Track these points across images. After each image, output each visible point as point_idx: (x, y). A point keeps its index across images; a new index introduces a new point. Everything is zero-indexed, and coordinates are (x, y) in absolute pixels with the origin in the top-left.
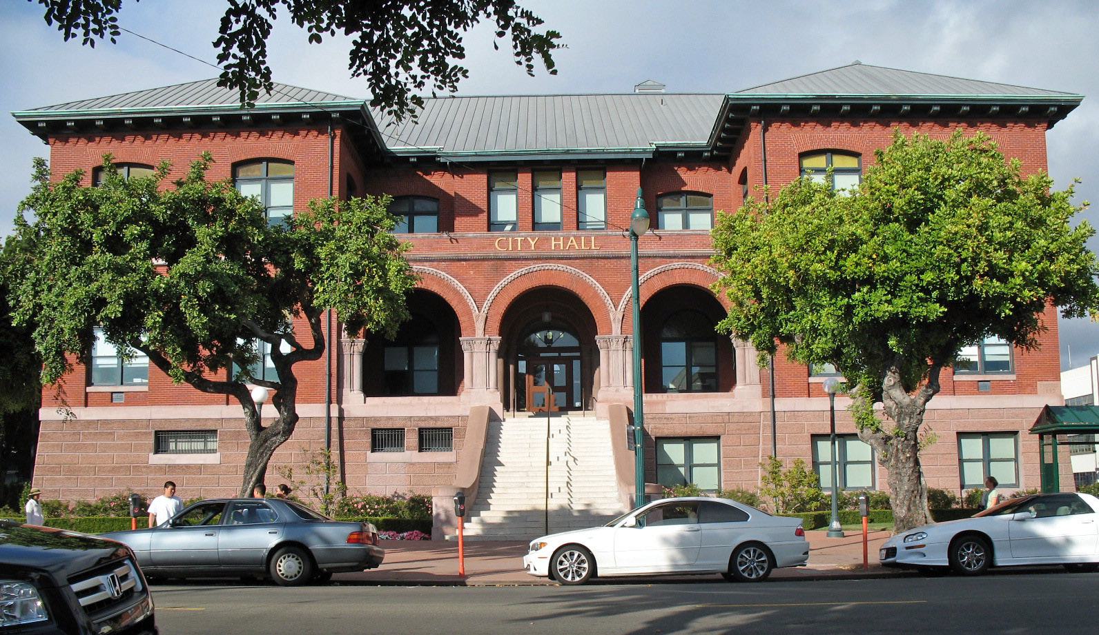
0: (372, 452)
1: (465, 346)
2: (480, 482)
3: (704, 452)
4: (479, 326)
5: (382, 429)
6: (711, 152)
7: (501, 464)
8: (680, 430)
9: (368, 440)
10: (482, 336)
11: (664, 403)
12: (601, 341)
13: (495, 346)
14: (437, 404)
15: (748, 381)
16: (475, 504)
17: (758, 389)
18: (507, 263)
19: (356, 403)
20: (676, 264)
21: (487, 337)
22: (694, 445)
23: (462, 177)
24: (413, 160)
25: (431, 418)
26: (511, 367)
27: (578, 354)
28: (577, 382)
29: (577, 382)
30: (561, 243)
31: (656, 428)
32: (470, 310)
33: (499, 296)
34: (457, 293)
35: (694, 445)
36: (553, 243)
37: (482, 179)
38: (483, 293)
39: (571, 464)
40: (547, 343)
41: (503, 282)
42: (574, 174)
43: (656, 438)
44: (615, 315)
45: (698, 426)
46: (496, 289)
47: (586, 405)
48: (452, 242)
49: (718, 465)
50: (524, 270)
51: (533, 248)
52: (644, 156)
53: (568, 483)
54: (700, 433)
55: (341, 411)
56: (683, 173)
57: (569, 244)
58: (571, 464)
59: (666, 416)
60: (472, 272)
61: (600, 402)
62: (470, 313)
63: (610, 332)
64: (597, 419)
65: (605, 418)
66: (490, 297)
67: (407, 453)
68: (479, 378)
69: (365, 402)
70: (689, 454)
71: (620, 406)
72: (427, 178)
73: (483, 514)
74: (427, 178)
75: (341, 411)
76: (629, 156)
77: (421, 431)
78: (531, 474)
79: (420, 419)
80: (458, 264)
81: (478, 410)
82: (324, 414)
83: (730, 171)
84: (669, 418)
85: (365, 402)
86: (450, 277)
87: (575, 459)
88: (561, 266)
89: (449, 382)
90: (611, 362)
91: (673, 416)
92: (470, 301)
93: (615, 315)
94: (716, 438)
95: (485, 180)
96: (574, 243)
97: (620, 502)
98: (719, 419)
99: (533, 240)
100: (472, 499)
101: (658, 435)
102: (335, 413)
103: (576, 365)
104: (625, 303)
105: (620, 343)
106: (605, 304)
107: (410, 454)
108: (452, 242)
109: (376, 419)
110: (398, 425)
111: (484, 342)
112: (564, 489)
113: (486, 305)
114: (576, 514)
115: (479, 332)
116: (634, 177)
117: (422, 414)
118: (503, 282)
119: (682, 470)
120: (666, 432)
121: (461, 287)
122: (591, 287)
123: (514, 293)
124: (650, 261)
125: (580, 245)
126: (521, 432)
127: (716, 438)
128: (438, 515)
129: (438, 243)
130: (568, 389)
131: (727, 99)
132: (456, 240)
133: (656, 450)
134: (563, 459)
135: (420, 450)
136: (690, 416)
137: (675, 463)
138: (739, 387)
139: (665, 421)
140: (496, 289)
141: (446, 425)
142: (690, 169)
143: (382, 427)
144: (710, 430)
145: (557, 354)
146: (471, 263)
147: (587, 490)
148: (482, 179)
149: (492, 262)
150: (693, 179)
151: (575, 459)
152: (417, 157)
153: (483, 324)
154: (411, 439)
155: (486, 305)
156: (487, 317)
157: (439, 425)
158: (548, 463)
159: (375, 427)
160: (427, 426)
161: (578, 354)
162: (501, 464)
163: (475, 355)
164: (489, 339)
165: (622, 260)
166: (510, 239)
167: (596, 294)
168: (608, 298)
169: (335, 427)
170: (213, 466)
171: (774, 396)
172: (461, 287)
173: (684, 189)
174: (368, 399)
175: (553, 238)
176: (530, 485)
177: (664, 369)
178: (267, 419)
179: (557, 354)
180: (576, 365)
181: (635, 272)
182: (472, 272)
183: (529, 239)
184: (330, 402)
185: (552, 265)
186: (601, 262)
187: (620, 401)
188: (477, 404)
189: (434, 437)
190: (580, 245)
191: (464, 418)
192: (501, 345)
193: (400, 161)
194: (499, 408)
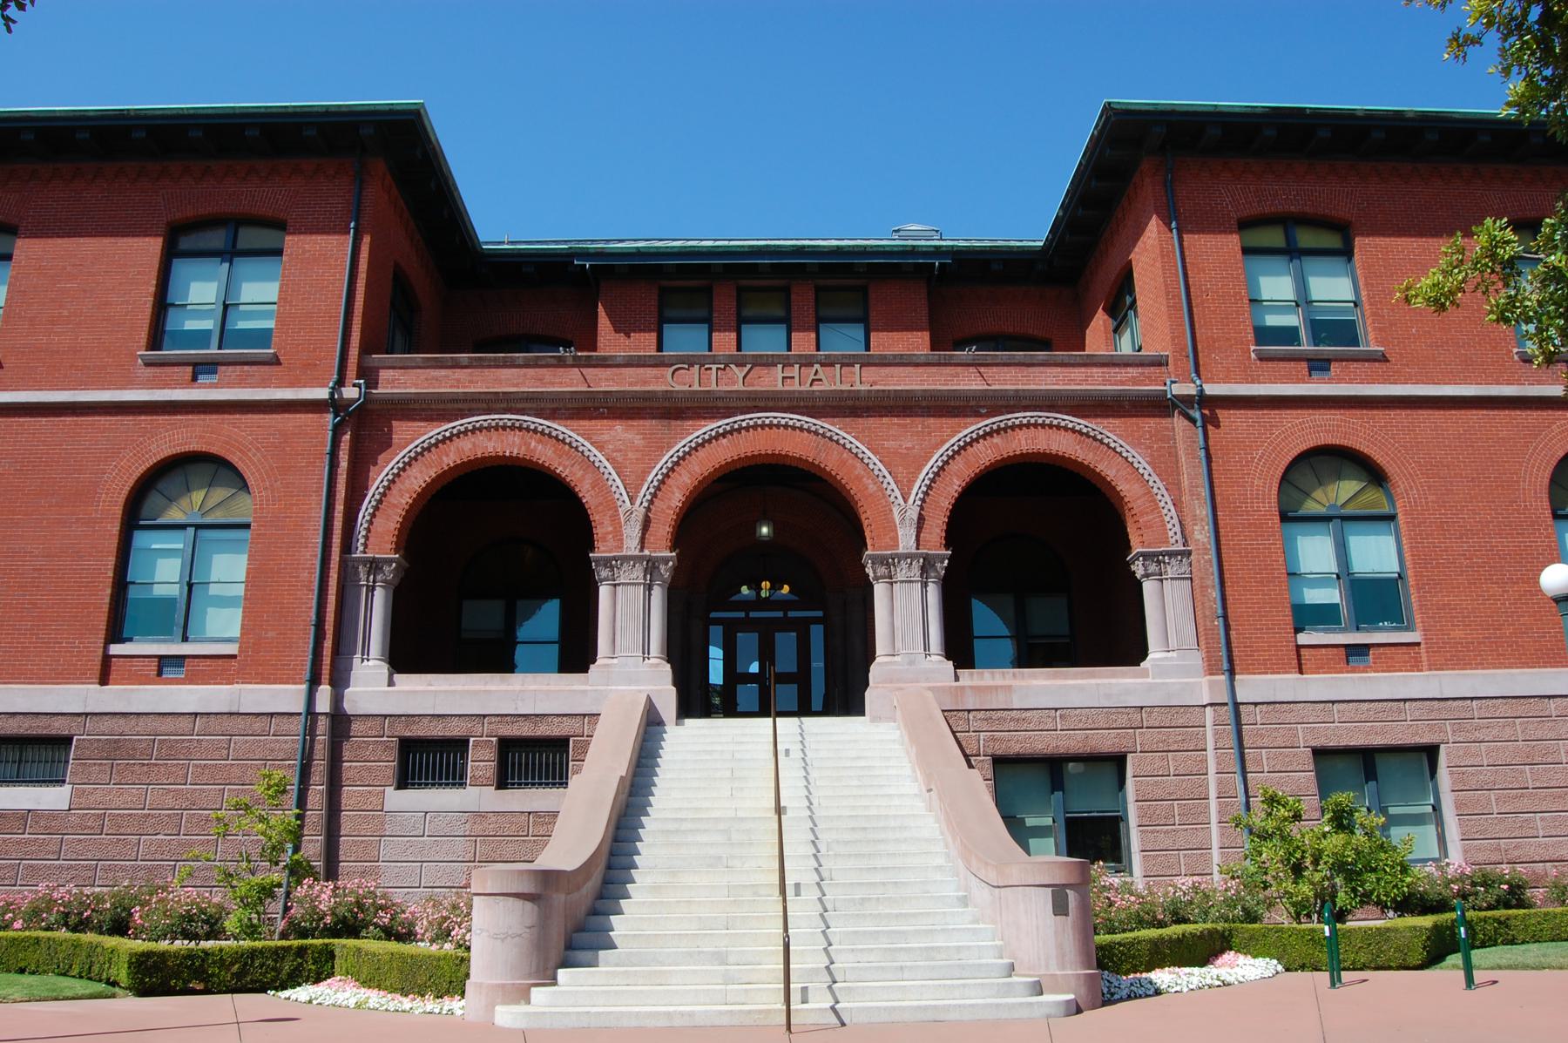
0: (399, 788)
4: (632, 533)
9: (388, 765)
15: (1173, 643)
17: (1196, 659)
19: (373, 687)
27: (820, 614)
31: (994, 739)
32: (614, 501)
46: (666, 460)
55: (337, 700)
66: (653, 476)
68: (630, 636)
75: (337, 700)
82: (300, 707)
89: (577, 653)
98: (1122, 720)
102: (323, 704)
103: (817, 632)
107: (476, 796)
110: (455, 730)
122: (859, 456)
126: (719, 760)
135: (502, 784)
138: (1155, 654)
145: (780, 614)
154: (481, 761)
155: (645, 491)
157: (543, 730)
161: (820, 614)
169: (322, 738)
170: (53, 815)
171: (1232, 672)
174: (397, 677)
178: (1455, 967)
179: (780, 614)
180: (817, 632)
181: (778, 898)
184: (314, 681)
189: (536, 758)
194: (667, 700)
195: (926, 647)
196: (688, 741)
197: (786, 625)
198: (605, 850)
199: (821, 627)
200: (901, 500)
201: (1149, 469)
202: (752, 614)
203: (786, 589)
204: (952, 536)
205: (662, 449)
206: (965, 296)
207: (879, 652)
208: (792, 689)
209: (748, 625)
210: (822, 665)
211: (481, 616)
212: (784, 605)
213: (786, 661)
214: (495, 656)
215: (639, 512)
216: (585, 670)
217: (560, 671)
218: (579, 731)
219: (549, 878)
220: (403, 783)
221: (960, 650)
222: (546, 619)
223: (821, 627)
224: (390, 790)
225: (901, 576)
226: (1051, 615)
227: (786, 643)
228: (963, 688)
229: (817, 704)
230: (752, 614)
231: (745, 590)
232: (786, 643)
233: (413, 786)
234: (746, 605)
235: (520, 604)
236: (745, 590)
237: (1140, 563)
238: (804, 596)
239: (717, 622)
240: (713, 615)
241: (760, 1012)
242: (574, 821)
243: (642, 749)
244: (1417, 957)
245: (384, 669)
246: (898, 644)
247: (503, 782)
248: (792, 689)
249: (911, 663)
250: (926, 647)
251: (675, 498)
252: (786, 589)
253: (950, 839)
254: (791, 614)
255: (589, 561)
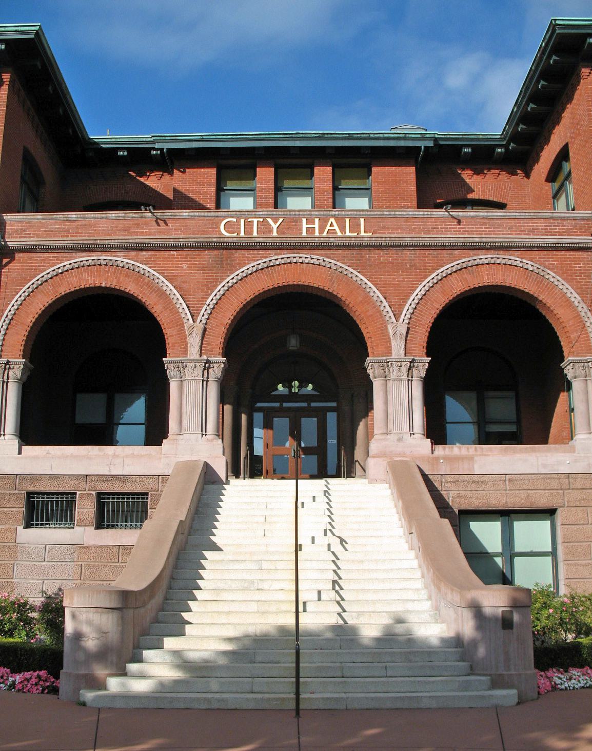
1: (171, 372)
2: (172, 578)
3: (532, 534)
4: (194, 342)
5: (43, 494)
6: (506, 146)
7: (215, 548)
8: (496, 501)
9: (19, 509)
10: (197, 357)
11: (471, 459)
12: (376, 365)
13: (216, 372)
14: (127, 456)
16: (156, 621)
18: (237, 254)
20: (484, 257)
21: (205, 357)
22: (515, 523)
23: (184, 172)
24: (121, 153)
25: (117, 477)
26: (244, 417)
27: (334, 404)
28: (332, 441)
29: (332, 441)
30: (316, 226)
31: (459, 496)
32: (181, 319)
33: (224, 300)
34: (162, 294)
35: (515, 523)
36: (305, 226)
37: (209, 175)
38: (200, 294)
39: (337, 547)
40: (296, 374)
41: (230, 279)
42: (329, 169)
43: (461, 512)
44: (396, 329)
45: (523, 494)
46: (220, 289)
47: (345, 467)
48: (158, 225)
49: (554, 554)
50: (261, 262)
51: (275, 234)
52: (422, 144)
53: (334, 582)
54: (526, 506)
56: (468, 176)
57: (328, 227)
58: (337, 547)
59: (475, 478)
60: (185, 266)
61: (374, 457)
62: (180, 324)
63: (389, 353)
64: (370, 482)
65: (383, 481)
66: (211, 300)
67: (78, 530)
68: (192, 420)
69: (20, 453)
70: (508, 537)
71: (405, 462)
72: (142, 179)
73: (170, 643)
74: (142, 179)
76: (402, 143)
77: (101, 497)
78: (265, 566)
79: (100, 477)
80: (166, 254)
81: (188, 466)
83: (528, 176)
84: (480, 480)
85: (20, 453)
86: (152, 272)
87: (342, 541)
88: (316, 257)
89: (156, 432)
90: (389, 397)
91: (485, 478)
92: (182, 305)
93: (396, 329)
94: (549, 513)
95: (214, 176)
96: (336, 227)
97: (436, 622)
98: (554, 484)
99: (275, 222)
100: (155, 609)
101: (463, 507)
103: (332, 418)
104: (411, 311)
105: (404, 369)
106: (380, 312)
107: (83, 533)
108: (158, 225)
109: (35, 478)
111: (199, 366)
112: (329, 595)
113: (204, 312)
114: (366, 642)
115: (193, 352)
116: (408, 174)
117: (104, 471)
118: (230, 279)
119: (499, 560)
120: (476, 503)
121: (168, 287)
122: (360, 288)
123: (247, 294)
124: (445, 253)
125: (343, 230)
126: (251, 506)
127: (549, 513)
128: (78, 636)
129: (137, 225)
130: (320, 451)
131: (553, 26)
132: (164, 221)
133: (460, 528)
134: (322, 540)
135: (99, 526)
136: (511, 479)
137: (490, 551)
139: (474, 486)
140: (220, 289)
141: (138, 489)
142: (478, 172)
143: (43, 489)
144: (542, 501)
145: (305, 405)
146: (185, 253)
147: (370, 596)
148: (209, 175)
149: (215, 252)
150: (481, 184)
151: (342, 541)
152: (128, 149)
153: (198, 339)
154: (86, 509)
155: (204, 312)
156: (205, 330)
157: (128, 488)
158: (298, 548)
159: (33, 489)
160: (111, 490)
161: (334, 404)
162: (215, 548)
163: (185, 383)
164: (208, 362)
165: (405, 251)
166: (242, 221)
167: (367, 299)
168: (385, 303)
172: (168, 287)
173: (470, 196)
174: (25, 448)
175: (304, 220)
176: (265, 586)
177: (448, 426)
180: (332, 418)
182: (185, 266)
183: (269, 220)
185: (303, 256)
186: (375, 254)
187: (404, 455)
188: (187, 458)
189: (120, 506)
190: (343, 230)
191: (164, 477)
192: (227, 372)
193: (106, 157)
194: (220, 466)
195: (411, 427)
196: (240, 495)
197: (309, 412)
198: (168, 573)
199: (335, 414)
200: (393, 319)
201: (579, 298)
202: (285, 405)
203: (310, 386)
204: (431, 349)
205: (217, 281)
206: (440, 169)
207: (376, 432)
208: (314, 459)
209: (281, 412)
210: (329, 441)
211: (89, 408)
212: (308, 398)
213: (310, 437)
214: (101, 435)
215: (199, 327)
216: (159, 443)
217: (145, 445)
218: (155, 487)
219: (125, 595)
220: (28, 526)
221: (437, 431)
222: (137, 409)
223: (335, 414)
224: (20, 529)
225: (393, 375)
226: (502, 407)
227: (309, 425)
228: (437, 459)
229: (331, 468)
230: (285, 405)
231: (280, 387)
232: (309, 425)
233: (37, 526)
234: (281, 398)
235: (118, 398)
236: (280, 387)
237: (569, 367)
238: (323, 393)
239: (260, 410)
240: (259, 405)
241: (277, 699)
242: (139, 553)
243: (199, 500)
244: (465, 552)
245: (16, 442)
246: (391, 426)
247: (100, 523)
248: (314, 459)
249: (400, 440)
250: (411, 427)
251: (227, 316)
252: (310, 386)
253: (425, 571)
254: (313, 404)
255: (163, 364)
